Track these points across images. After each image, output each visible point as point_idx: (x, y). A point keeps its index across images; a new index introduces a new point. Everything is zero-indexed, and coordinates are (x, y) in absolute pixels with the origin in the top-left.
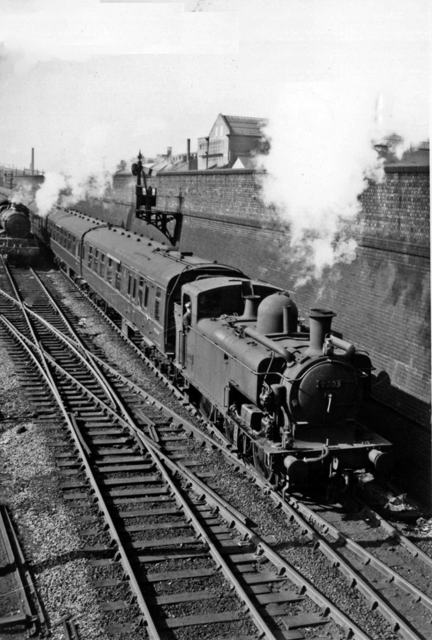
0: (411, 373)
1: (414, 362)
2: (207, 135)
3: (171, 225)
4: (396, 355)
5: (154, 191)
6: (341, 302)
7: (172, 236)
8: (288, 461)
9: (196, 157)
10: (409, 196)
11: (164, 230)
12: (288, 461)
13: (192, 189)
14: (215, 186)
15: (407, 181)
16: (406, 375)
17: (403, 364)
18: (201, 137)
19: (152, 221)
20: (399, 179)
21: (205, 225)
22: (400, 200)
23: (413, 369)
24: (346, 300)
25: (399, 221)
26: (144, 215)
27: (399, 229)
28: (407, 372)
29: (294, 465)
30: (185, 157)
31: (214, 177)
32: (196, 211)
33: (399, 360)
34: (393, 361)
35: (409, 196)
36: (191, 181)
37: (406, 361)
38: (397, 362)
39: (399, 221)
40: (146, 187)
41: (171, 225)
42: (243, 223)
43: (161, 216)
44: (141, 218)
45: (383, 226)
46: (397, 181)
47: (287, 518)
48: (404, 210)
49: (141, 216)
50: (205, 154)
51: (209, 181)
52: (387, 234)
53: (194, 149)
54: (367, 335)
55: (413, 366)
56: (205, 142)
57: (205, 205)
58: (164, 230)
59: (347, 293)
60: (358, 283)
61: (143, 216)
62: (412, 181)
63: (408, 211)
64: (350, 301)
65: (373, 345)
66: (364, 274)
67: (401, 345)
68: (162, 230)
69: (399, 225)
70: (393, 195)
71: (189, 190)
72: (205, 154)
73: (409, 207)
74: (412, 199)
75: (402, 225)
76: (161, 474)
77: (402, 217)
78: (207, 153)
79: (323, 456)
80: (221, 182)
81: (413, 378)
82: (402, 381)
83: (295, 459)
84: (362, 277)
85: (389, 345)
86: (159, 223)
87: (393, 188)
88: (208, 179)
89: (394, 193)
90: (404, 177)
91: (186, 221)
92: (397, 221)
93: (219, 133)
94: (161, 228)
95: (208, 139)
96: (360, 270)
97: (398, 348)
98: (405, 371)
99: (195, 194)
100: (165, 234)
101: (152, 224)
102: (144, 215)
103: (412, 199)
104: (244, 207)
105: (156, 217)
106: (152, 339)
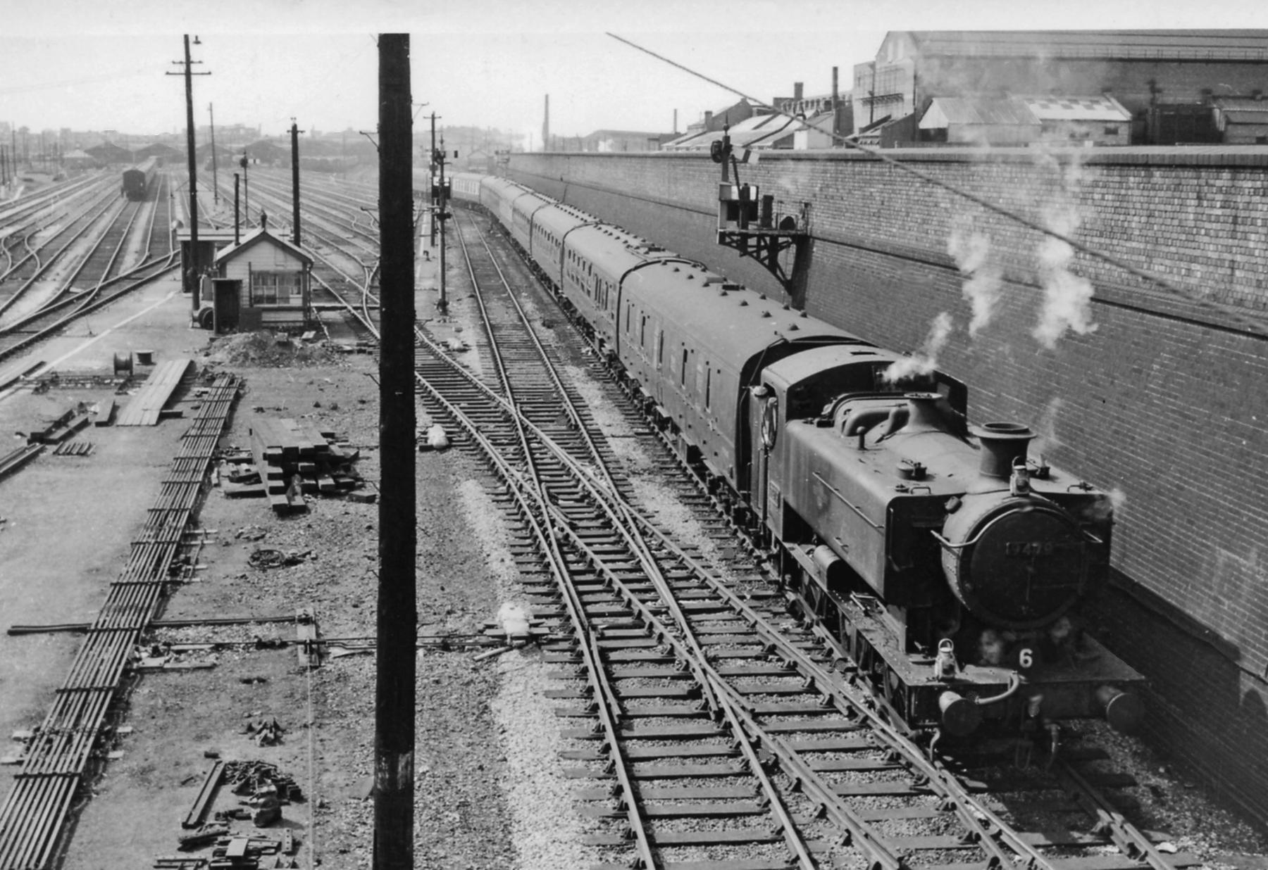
0: (1253, 578)
1: (1259, 556)
2: (871, 58)
3: (787, 258)
4: (1221, 538)
5: (753, 191)
6: (1112, 424)
7: (789, 278)
8: (947, 700)
9: (850, 101)
10: (1253, 214)
11: (773, 266)
12: (947, 700)
13: (828, 186)
14: (869, 183)
15: (1250, 184)
16: (1242, 581)
17: (1237, 557)
18: (861, 62)
19: (750, 250)
20: (1233, 179)
21: (852, 257)
22: (1235, 223)
23: (1257, 568)
24: (1123, 421)
25: (1233, 266)
26: (735, 238)
27: (1231, 282)
28: (1245, 574)
29: (954, 706)
30: (827, 103)
31: (869, 165)
32: (833, 228)
33: (1226, 548)
34: (1214, 551)
35: (1253, 214)
36: (825, 172)
37: (1244, 552)
38: (1224, 552)
39: (1233, 266)
40: (738, 184)
41: (787, 258)
42: (923, 257)
43: (768, 239)
44: (729, 244)
45: (1199, 274)
46: (1229, 183)
47: (824, 640)
48: (1242, 243)
49: (728, 240)
50: (867, 96)
51: (860, 173)
52: (1207, 291)
53: (846, 86)
54: (1163, 495)
55: (1258, 564)
56: (868, 71)
57: (850, 219)
58: (773, 266)
59: (1124, 408)
60: (1146, 388)
61: (733, 241)
62: (1259, 184)
63: (1251, 245)
64: (1129, 423)
65: (1175, 516)
66: (1160, 371)
67: (1234, 519)
68: (768, 267)
69: (1232, 275)
70: (1219, 212)
71: (821, 189)
72: (867, 96)
73: (1253, 237)
74: (1259, 222)
75: (1238, 273)
76: (748, 761)
77: (1238, 258)
78: (871, 93)
79: (1010, 691)
80: (882, 174)
81: (1256, 589)
82: (1234, 592)
83: (957, 697)
84: (1155, 377)
85: (1209, 516)
86: (764, 253)
87: (1220, 197)
88: (857, 169)
89: (1222, 207)
90: (1242, 176)
91: (817, 249)
92: (1227, 264)
93: (895, 53)
94: (767, 262)
95: (872, 66)
96: (1152, 362)
97: (1228, 525)
98: (1240, 572)
99: (832, 197)
100: (775, 273)
101: (750, 254)
102: (735, 238)
103: (1259, 222)
104: (926, 227)
105: (759, 242)
106: (717, 464)
